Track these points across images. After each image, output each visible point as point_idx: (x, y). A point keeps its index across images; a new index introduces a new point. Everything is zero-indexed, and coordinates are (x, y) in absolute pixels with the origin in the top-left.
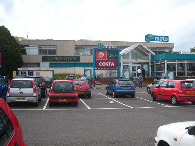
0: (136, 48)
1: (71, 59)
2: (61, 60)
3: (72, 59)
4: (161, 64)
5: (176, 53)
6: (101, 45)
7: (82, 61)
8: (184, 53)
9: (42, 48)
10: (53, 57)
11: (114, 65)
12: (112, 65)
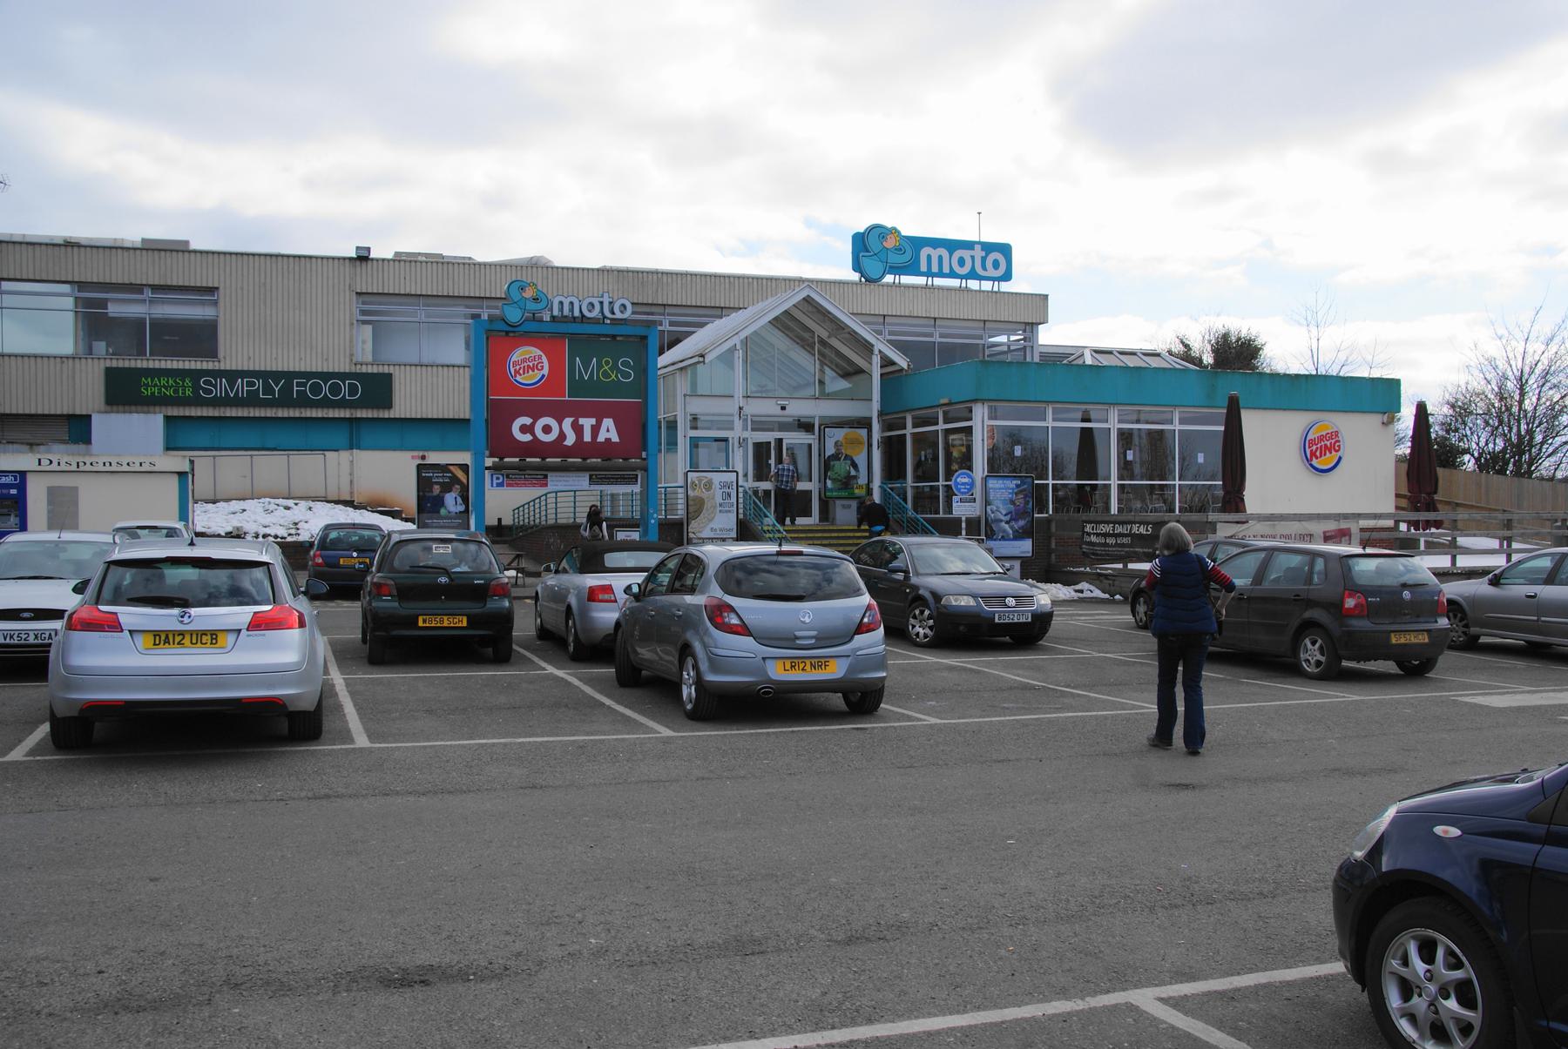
0: (784, 323)
1: (326, 389)
2: (252, 400)
3: (335, 389)
4: (948, 432)
5: (1061, 362)
6: (529, 294)
7: (406, 403)
8: (1105, 361)
9: (103, 304)
10: (196, 375)
11: (615, 438)
12: (601, 438)
